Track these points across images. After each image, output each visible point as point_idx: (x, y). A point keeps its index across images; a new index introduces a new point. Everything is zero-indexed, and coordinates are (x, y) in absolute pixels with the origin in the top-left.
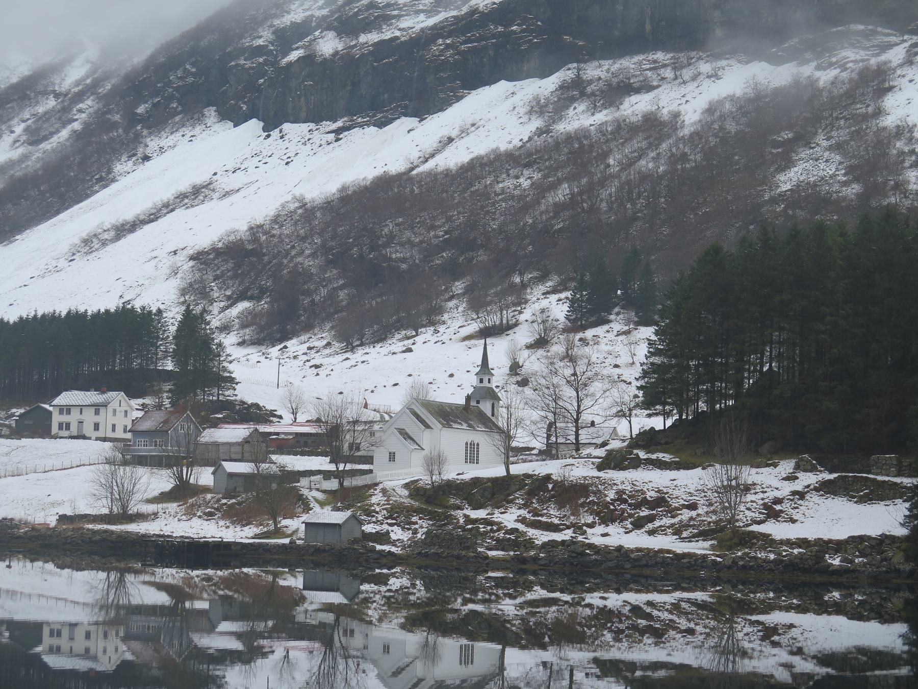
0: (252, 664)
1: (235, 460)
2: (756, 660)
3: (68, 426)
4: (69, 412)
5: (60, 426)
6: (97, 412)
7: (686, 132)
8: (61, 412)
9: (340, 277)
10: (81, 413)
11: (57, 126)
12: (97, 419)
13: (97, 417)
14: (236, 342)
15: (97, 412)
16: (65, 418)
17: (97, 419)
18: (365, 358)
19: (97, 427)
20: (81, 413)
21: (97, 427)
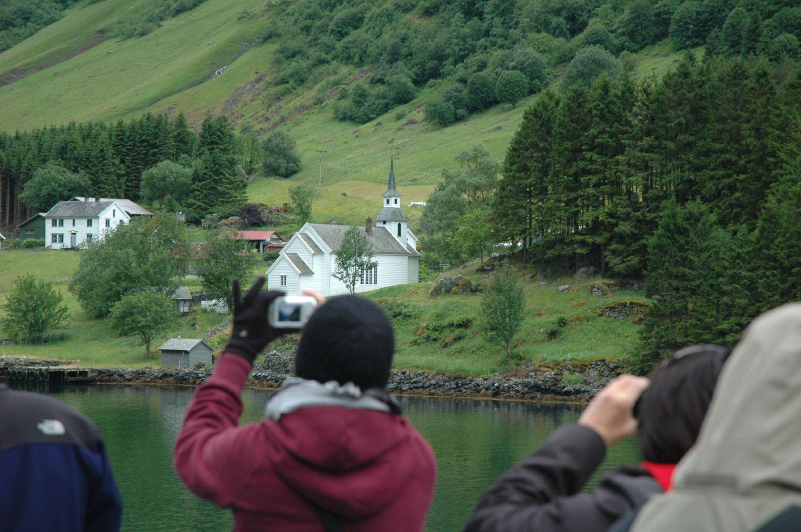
4: (62, 224)
6: (89, 223)
8: (54, 224)
13: (89, 228)
16: (58, 230)
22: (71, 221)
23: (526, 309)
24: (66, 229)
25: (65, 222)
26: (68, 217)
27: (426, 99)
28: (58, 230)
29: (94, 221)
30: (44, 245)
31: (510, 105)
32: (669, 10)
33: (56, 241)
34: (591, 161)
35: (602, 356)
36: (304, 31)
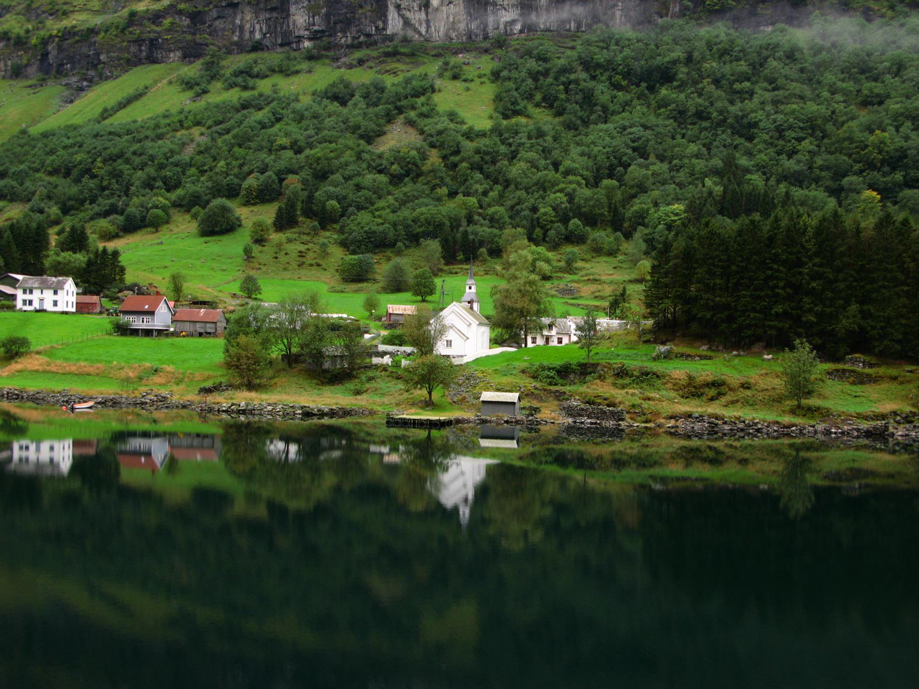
0: (809, 506)
1: (507, 391)
2: (29, 189)
3: (31, 303)
4: (31, 292)
5: (24, 302)
6: (55, 293)
7: (438, 239)
8: (25, 292)
9: (723, 160)
10: (42, 293)
11: (452, 132)
12: (55, 298)
13: (55, 299)
14: (180, 90)
15: (55, 293)
16: (28, 297)
17: (55, 298)
18: (70, 294)
19: (55, 303)
20: (42, 293)
21: (55, 303)
22: (40, 291)
23: (446, 279)
24: (36, 296)
25: (34, 291)
26: (36, 288)
27: (112, 149)
28: (28, 297)
29: (59, 292)
30: (15, 306)
31: (154, 230)
32: (425, 283)
33: (26, 304)
34: (778, 271)
35: (33, 341)
36: (286, 361)
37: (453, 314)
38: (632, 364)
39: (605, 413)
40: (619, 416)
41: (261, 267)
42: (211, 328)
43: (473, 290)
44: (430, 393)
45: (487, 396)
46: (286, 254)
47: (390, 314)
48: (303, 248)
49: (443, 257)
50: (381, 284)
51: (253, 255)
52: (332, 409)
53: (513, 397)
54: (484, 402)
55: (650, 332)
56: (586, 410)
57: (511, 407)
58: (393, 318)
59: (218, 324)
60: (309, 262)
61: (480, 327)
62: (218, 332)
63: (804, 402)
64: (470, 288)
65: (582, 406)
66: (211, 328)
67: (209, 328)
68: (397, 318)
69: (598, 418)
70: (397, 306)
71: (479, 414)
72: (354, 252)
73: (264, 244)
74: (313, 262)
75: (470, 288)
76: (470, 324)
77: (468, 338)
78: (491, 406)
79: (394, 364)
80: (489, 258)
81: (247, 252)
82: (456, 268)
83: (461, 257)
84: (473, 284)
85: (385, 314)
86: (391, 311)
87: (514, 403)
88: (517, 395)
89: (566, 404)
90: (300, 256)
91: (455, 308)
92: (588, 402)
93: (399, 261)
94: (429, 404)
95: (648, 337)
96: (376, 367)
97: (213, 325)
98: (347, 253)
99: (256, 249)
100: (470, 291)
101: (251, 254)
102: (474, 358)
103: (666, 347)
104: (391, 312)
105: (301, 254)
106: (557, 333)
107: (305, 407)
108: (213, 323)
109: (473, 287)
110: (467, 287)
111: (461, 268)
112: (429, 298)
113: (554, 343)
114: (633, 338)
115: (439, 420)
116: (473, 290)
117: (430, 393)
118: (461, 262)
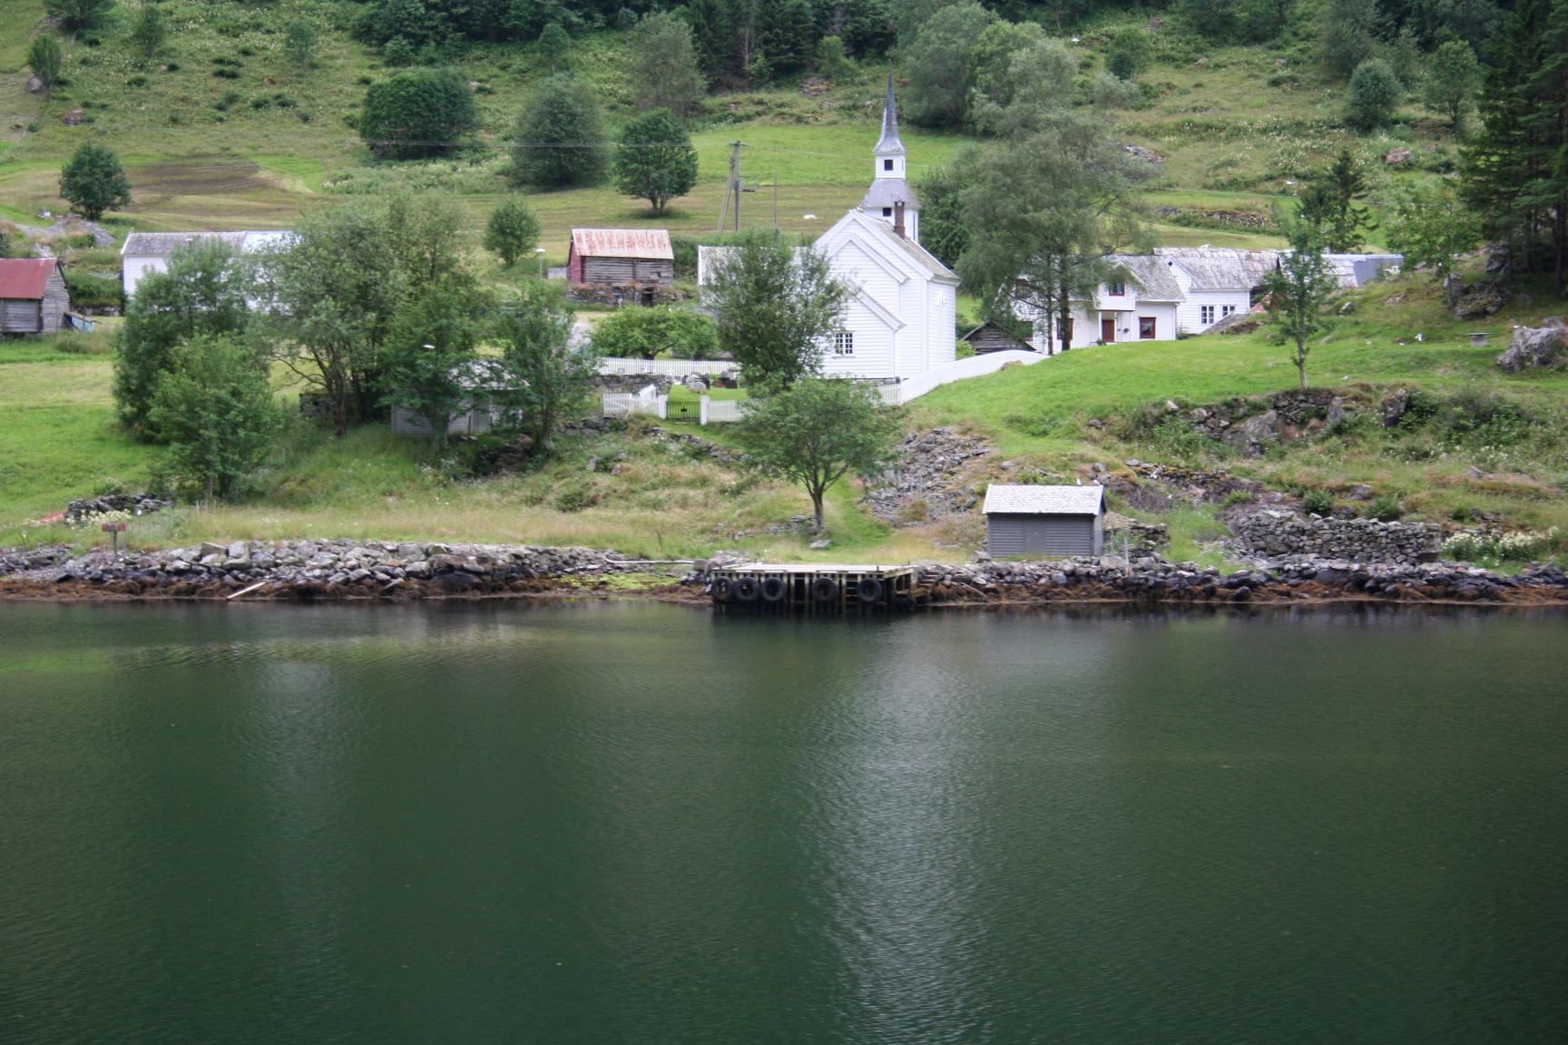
37: (851, 250)
38: (1441, 384)
39: (1373, 538)
40: (1421, 546)
41: (90, 113)
42: (25, 319)
43: (899, 171)
44: (817, 495)
45: (1003, 498)
46: (173, 68)
47: (583, 258)
48: (224, 47)
49: (703, 66)
50: (504, 160)
51: (61, 74)
52: (517, 557)
53: (1082, 498)
54: (994, 517)
55: (1484, 285)
56: (1312, 534)
57: (1082, 528)
58: (591, 269)
59: (48, 306)
60: (254, 95)
61: (933, 286)
62: (46, 330)
63: (1352, 522)
64: (889, 165)
65: (1299, 521)
66: (25, 319)
67: (17, 317)
68: (605, 271)
69: (1351, 557)
70: (605, 232)
71: (983, 554)
72: (397, 60)
73: (89, 35)
74: (268, 92)
75: (889, 165)
76: (908, 279)
77: (1204, 308)
78: (1017, 529)
79: (676, 412)
80: (851, 62)
81: (42, 60)
82: (742, 100)
83: (756, 62)
84: (898, 153)
85: (563, 257)
86: (583, 249)
87: (1089, 518)
88: (1098, 491)
89: (1242, 517)
90: (221, 74)
91: (855, 229)
92: (1312, 508)
93: (560, 86)
94: (810, 531)
95: (1482, 299)
96: (616, 425)
97: (29, 310)
98: (378, 61)
99: (70, 51)
100: (889, 174)
101: (54, 71)
102: (931, 386)
103: (1544, 331)
104: (587, 252)
105: (226, 70)
106: (1139, 304)
107: (437, 550)
108: (30, 300)
109: (899, 163)
110: (880, 164)
111: (760, 103)
112: (675, 202)
113: (1128, 332)
114: (1434, 306)
115: (879, 575)
116: (899, 171)
117: (817, 495)
118: (757, 82)
